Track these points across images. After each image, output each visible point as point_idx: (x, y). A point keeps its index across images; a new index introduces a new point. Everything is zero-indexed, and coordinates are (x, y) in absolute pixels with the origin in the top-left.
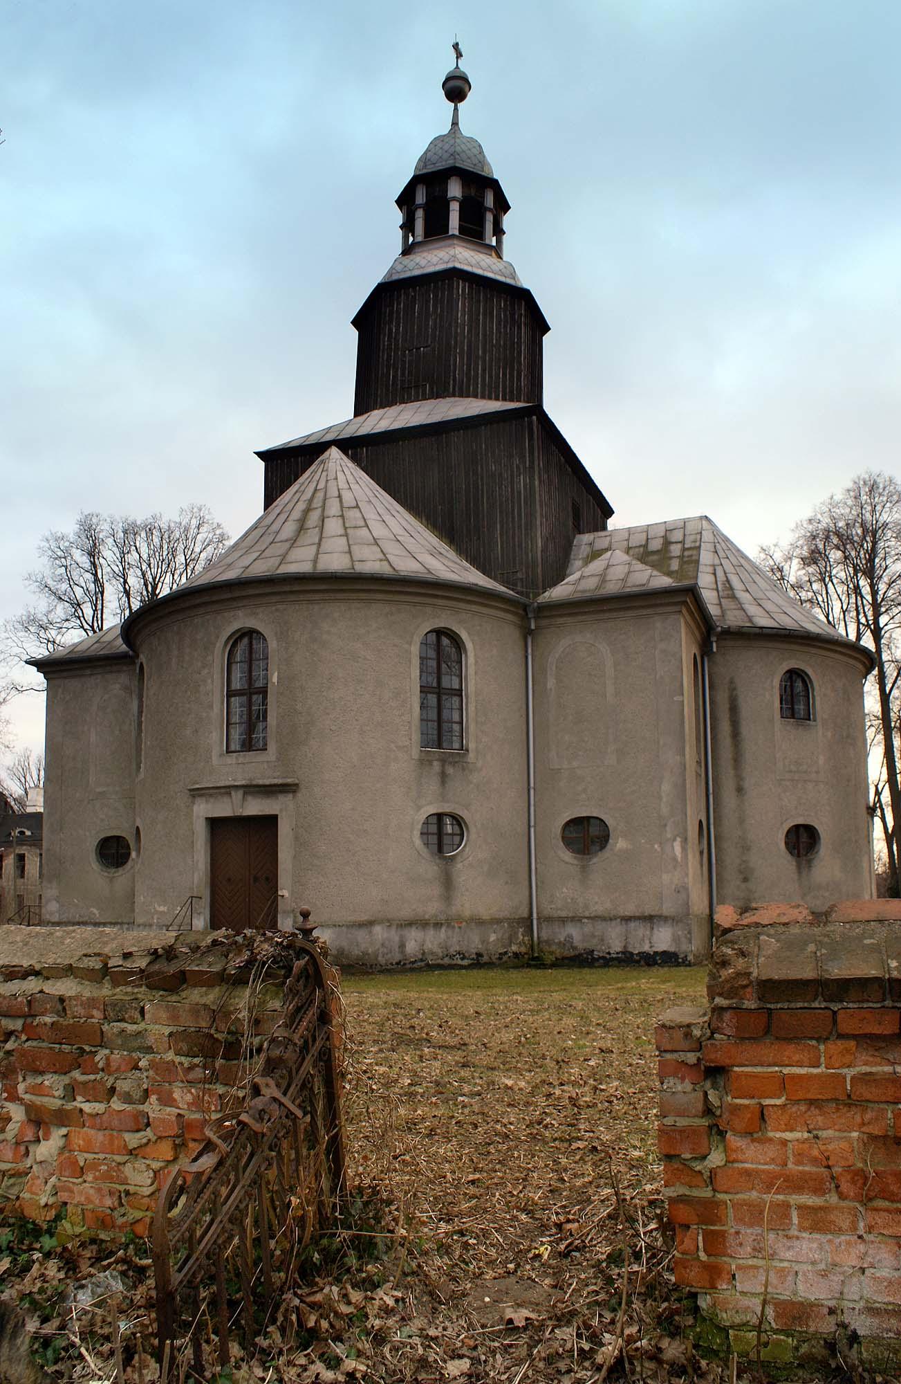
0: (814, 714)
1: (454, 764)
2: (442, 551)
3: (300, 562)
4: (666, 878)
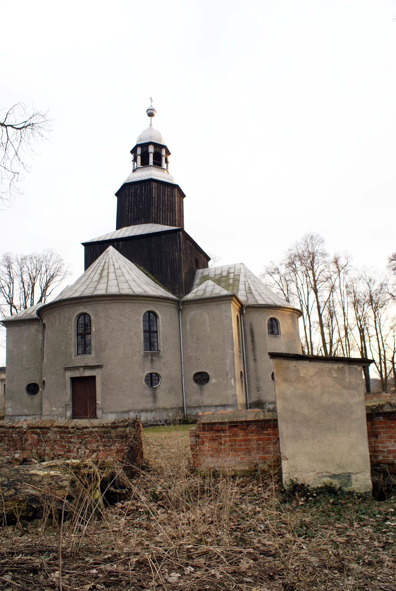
0: (280, 332)
1: (155, 356)
2: (150, 283)
3: (101, 291)
4: (229, 391)
